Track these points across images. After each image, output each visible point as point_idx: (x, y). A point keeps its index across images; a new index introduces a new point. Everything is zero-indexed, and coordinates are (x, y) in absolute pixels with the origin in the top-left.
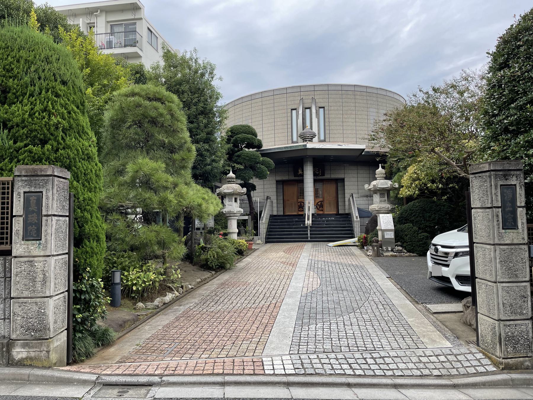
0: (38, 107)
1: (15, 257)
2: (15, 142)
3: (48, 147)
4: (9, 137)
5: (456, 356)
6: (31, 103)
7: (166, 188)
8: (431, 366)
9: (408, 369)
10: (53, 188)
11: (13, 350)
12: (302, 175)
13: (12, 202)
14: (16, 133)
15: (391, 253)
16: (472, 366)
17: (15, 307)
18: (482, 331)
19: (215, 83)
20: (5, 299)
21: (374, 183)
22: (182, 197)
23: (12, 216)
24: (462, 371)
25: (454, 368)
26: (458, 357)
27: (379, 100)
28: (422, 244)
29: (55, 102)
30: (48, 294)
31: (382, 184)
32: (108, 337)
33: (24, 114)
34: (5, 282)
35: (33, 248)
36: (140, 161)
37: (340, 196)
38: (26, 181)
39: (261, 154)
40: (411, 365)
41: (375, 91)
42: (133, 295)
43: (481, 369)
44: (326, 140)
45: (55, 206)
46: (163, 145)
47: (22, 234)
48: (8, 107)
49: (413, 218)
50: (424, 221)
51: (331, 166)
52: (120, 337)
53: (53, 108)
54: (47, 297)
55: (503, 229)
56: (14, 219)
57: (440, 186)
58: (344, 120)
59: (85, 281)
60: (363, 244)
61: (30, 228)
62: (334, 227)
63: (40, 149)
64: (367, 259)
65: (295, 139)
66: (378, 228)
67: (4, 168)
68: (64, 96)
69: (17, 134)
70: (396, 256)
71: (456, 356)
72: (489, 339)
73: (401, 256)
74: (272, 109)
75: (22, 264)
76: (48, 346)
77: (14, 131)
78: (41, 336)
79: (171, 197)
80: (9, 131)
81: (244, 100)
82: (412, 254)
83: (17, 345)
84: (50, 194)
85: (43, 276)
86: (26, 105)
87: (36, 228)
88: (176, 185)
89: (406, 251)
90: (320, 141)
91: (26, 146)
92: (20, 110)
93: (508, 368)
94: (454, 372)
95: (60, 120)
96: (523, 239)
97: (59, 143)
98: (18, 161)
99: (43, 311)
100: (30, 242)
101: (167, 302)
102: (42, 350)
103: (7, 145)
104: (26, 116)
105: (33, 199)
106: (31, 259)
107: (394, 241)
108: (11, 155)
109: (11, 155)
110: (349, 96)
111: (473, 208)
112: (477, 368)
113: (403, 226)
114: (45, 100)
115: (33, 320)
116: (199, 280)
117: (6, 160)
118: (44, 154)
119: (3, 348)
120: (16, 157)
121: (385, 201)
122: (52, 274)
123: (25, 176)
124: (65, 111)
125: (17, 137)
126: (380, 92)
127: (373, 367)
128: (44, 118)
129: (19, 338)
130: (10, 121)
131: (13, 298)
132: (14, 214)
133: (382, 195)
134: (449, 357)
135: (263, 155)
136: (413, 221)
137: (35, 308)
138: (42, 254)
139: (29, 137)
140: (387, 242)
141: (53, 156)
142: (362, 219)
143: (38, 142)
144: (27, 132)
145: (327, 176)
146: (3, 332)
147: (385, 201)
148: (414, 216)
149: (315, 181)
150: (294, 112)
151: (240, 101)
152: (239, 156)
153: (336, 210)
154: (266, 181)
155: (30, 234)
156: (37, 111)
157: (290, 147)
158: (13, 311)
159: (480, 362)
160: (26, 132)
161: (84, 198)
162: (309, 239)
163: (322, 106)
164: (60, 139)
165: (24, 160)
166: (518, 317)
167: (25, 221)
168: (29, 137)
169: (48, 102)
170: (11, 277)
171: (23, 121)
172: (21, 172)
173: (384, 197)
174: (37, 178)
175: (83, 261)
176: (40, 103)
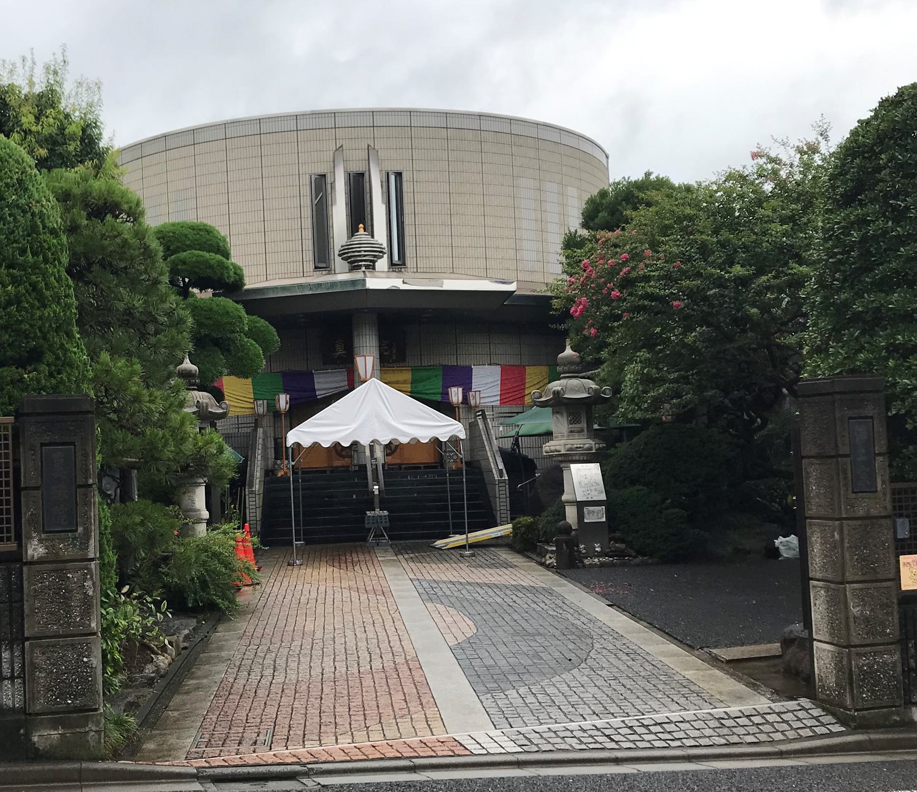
5: (779, 714)
8: (741, 731)
9: (705, 737)
16: (806, 727)
18: (820, 670)
24: (791, 734)
25: (778, 731)
26: (782, 716)
40: (708, 732)
43: (821, 730)
46: (128, 319)
55: (854, 492)
56: (23, 493)
60: (525, 544)
64: (551, 576)
66: (564, 497)
70: (612, 565)
71: (779, 714)
72: (831, 681)
73: (624, 565)
93: (861, 726)
94: (778, 736)
96: (885, 508)
111: (803, 457)
112: (817, 724)
127: (646, 737)
131: (28, 639)
134: (768, 717)
147: (581, 431)
151: (161, 146)
159: (818, 721)
166: (879, 639)
173: (579, 422)
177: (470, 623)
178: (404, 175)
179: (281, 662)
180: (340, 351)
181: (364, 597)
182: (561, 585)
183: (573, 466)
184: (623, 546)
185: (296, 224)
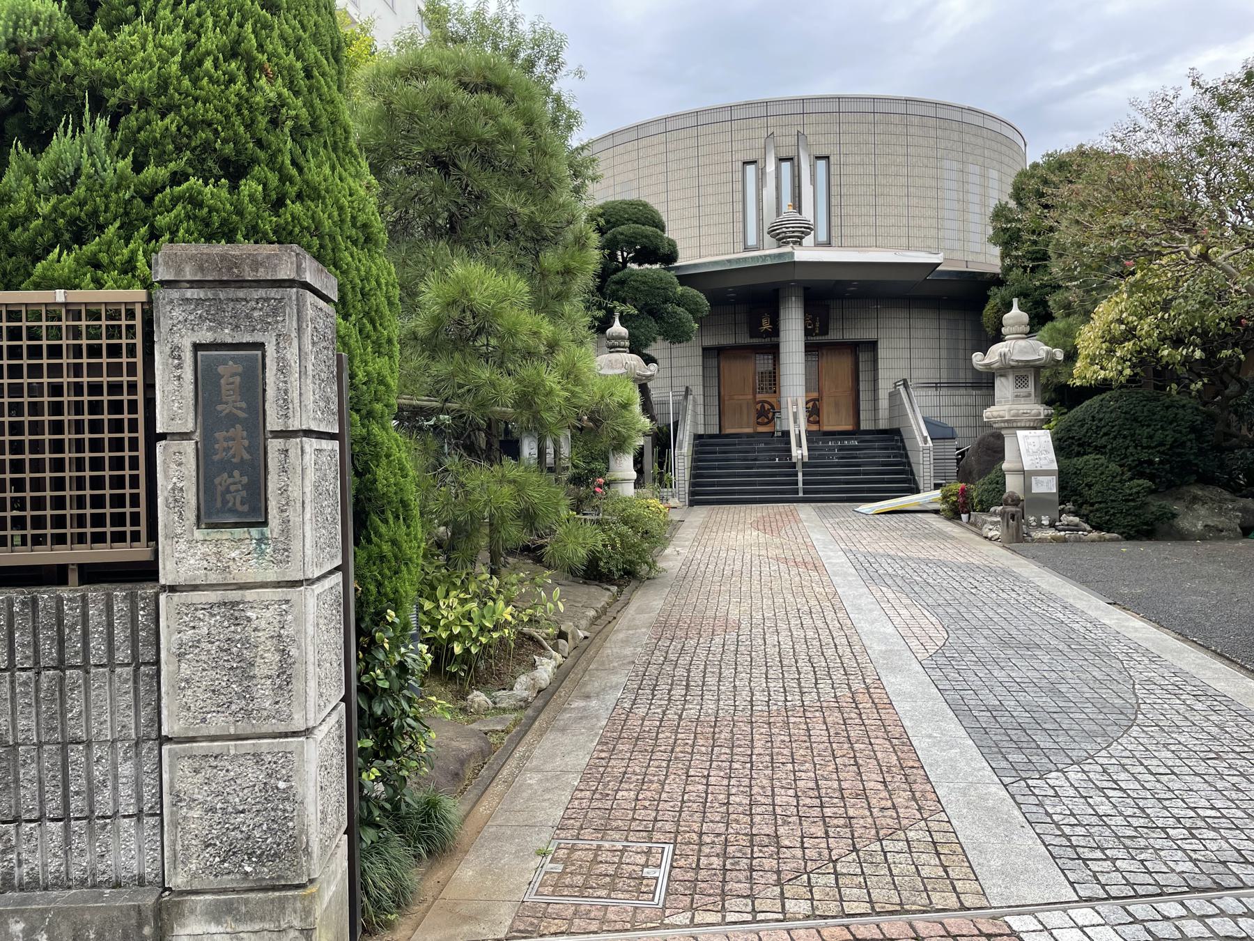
0: (211, 40)
1: (173, 589)
2: (138, 167)
3: (250, 186)
4: (116, 145)
6: (186, 27)
7: (529, 354)
10: (299, 330)
11: (178, 930)
12: (775, 331)
13: (150, 387)
14: (140, 129)
15: (1051, 533)
17: (179, 773)
19: (563, 85)
20: (137, 744)
21: (997, 350)
22: (577, 381)
23: (153, 438)
27: (967, 138)
28: (1136, 508)
29: (264, 27)
30: (298, 725)
31: (1022, 351)
32: (444, 827)
33: (164, 61)
34: (135, 682)
35: (237, 554)
36: (459, 270)
37: (863, 386)
38: (199, 302)
39: (678, 277)
41: (957, 116)
42: (454, 669)
44: (833, 243)
45: (310, 398)
46: (509, 230)
47: (193, 502)
48: (104, 35)
49: (1103, 441)
50: (1136, 447)
51: (844, 304)
52: (466, 816)
53: (261, 47)
54: (295, 734)
56: (160, 446)
57: (1198, 354)
58: (879, 190)
59: (381, 656)
61: (222, 480)
62: (864, 467)
63: (224, 194)
65: (752, 241)
66: (1005, 466)
67: (104, 258)
68: (289, 10)
69: (142, 136)
70: (1065, 540)
73: (1079, 540)
74: (694, 163)
75: (200, 614)
76: (307, 912)
77: (132, 121)
78: (279, 878)
79: (551, 380)
80: (113, 126)
81: (618, 140)
82: (1108, 536)
83: (192, 912)
84: (292, 354)
85: (277, 657)
86: (169, 30)
87: (245, 480)
88: (553, 346)
89: (1088, 528)
90: (818, 244)
91: (177, 178)
92: (150, 46)
95: (285, 92)
97: (284, 178)
98: (154, 235)
99: (282, 785)
100: (225, 534)
101: (544, 686)
102: (284, 926)
103: (110, 172)
104: (174, 68)
105: (229, 368)
106: (231, 600)
107: (1057, 498)
108: (127, 214)
109: (127, 214)
110: (892, 128)
113: (1079, 462)
114: (231, 15)
115: (248, 819)
116: (592, 613)
117: (111, 230)
118: (240, 213)
119: (140, 926)
120: (144, 221)
121: (1029, 395)
122: (310, 648)
123: (193, 284)
124: (299, 65)
125: (144, 149)
126: (968, 118)
128: (232, 80)
129: (196, 885)
130: (114, 84)
131: (169, 740)
132: (159, 430)
133: (1020, 381)
135: (685, 280)
136: (1105, 447)
137: (254, 775)
138: (272, 575)
139: (187, 146)
140: (1040, 502)
141: (268, 223)
142: (940, 443)
143: (216, 170)
144: (179, 129)
145: (834, 336)
146: (135, 863)
147: (1029, 395)
148: (1105, 434)
149: (810, 348)
150: (751, 169)
151: (609, 143)
152: (622, 282)
153: (851, 420)
154: (678, 349)
155: (225, 502)
156: (208, 53)
157: (738, 260)
158: (172, 786)
160: (174, 128)
161: (368, 374)
162: (801, 495)
163: (824, 153)
164: (288, 162)
165: (174, 233)
167: (204, 458)
168: (187, 146)
169: (241, 26)
170: (157, 662)
171: (163, 85)
172: (179, 270)
174: (241, 293)
175: (373, 588)
176: (215, 26)
177: (933, 620)
178: (832, 158)
179: (696, 675)
180: (766, 325)
181: (794, 571)
182: (1020, 565)
183: (1020, 433)
184: (1077, 520)
185: (728, 208)
